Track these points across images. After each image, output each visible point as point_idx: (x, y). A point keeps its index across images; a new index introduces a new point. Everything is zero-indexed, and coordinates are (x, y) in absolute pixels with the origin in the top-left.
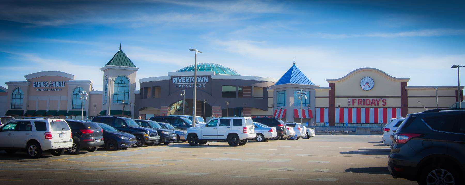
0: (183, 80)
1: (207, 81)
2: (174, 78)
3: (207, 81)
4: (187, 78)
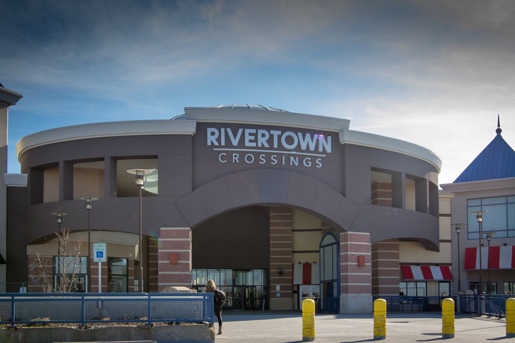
0: (247, 138)
1: (329, 150)
2: (209, 130)
3: (297, 164)
4: (260, 132)
